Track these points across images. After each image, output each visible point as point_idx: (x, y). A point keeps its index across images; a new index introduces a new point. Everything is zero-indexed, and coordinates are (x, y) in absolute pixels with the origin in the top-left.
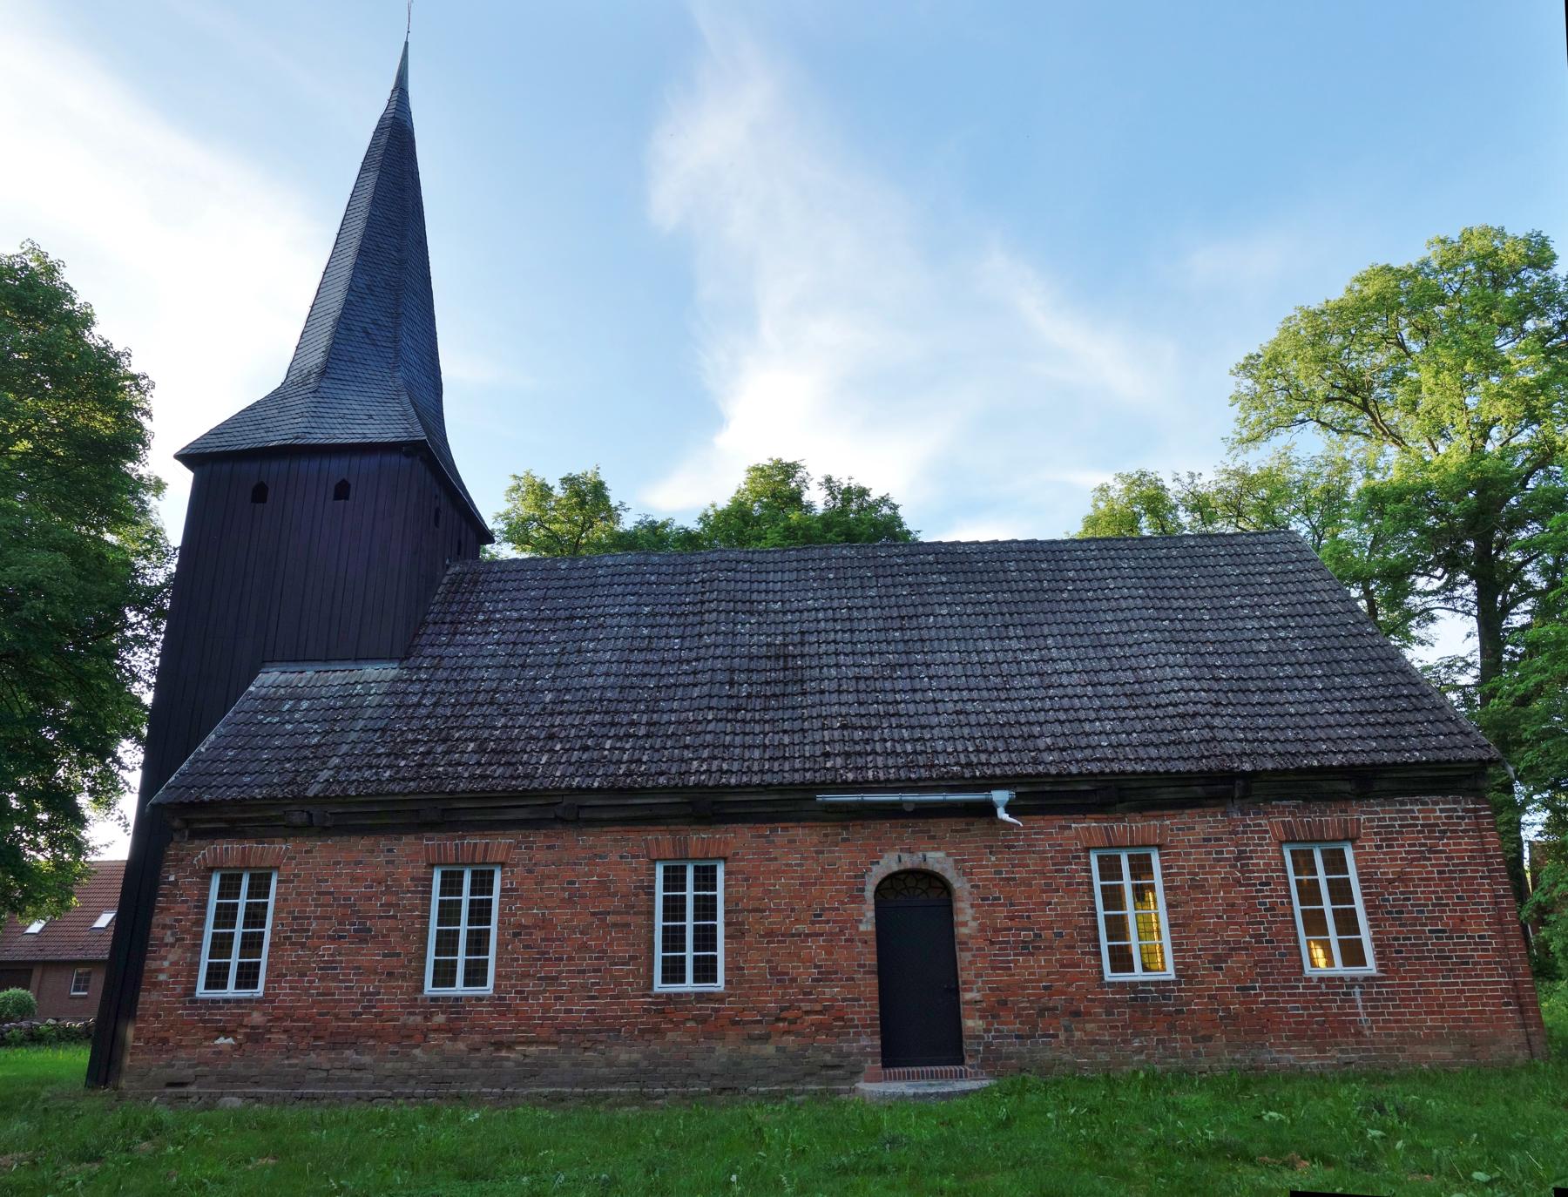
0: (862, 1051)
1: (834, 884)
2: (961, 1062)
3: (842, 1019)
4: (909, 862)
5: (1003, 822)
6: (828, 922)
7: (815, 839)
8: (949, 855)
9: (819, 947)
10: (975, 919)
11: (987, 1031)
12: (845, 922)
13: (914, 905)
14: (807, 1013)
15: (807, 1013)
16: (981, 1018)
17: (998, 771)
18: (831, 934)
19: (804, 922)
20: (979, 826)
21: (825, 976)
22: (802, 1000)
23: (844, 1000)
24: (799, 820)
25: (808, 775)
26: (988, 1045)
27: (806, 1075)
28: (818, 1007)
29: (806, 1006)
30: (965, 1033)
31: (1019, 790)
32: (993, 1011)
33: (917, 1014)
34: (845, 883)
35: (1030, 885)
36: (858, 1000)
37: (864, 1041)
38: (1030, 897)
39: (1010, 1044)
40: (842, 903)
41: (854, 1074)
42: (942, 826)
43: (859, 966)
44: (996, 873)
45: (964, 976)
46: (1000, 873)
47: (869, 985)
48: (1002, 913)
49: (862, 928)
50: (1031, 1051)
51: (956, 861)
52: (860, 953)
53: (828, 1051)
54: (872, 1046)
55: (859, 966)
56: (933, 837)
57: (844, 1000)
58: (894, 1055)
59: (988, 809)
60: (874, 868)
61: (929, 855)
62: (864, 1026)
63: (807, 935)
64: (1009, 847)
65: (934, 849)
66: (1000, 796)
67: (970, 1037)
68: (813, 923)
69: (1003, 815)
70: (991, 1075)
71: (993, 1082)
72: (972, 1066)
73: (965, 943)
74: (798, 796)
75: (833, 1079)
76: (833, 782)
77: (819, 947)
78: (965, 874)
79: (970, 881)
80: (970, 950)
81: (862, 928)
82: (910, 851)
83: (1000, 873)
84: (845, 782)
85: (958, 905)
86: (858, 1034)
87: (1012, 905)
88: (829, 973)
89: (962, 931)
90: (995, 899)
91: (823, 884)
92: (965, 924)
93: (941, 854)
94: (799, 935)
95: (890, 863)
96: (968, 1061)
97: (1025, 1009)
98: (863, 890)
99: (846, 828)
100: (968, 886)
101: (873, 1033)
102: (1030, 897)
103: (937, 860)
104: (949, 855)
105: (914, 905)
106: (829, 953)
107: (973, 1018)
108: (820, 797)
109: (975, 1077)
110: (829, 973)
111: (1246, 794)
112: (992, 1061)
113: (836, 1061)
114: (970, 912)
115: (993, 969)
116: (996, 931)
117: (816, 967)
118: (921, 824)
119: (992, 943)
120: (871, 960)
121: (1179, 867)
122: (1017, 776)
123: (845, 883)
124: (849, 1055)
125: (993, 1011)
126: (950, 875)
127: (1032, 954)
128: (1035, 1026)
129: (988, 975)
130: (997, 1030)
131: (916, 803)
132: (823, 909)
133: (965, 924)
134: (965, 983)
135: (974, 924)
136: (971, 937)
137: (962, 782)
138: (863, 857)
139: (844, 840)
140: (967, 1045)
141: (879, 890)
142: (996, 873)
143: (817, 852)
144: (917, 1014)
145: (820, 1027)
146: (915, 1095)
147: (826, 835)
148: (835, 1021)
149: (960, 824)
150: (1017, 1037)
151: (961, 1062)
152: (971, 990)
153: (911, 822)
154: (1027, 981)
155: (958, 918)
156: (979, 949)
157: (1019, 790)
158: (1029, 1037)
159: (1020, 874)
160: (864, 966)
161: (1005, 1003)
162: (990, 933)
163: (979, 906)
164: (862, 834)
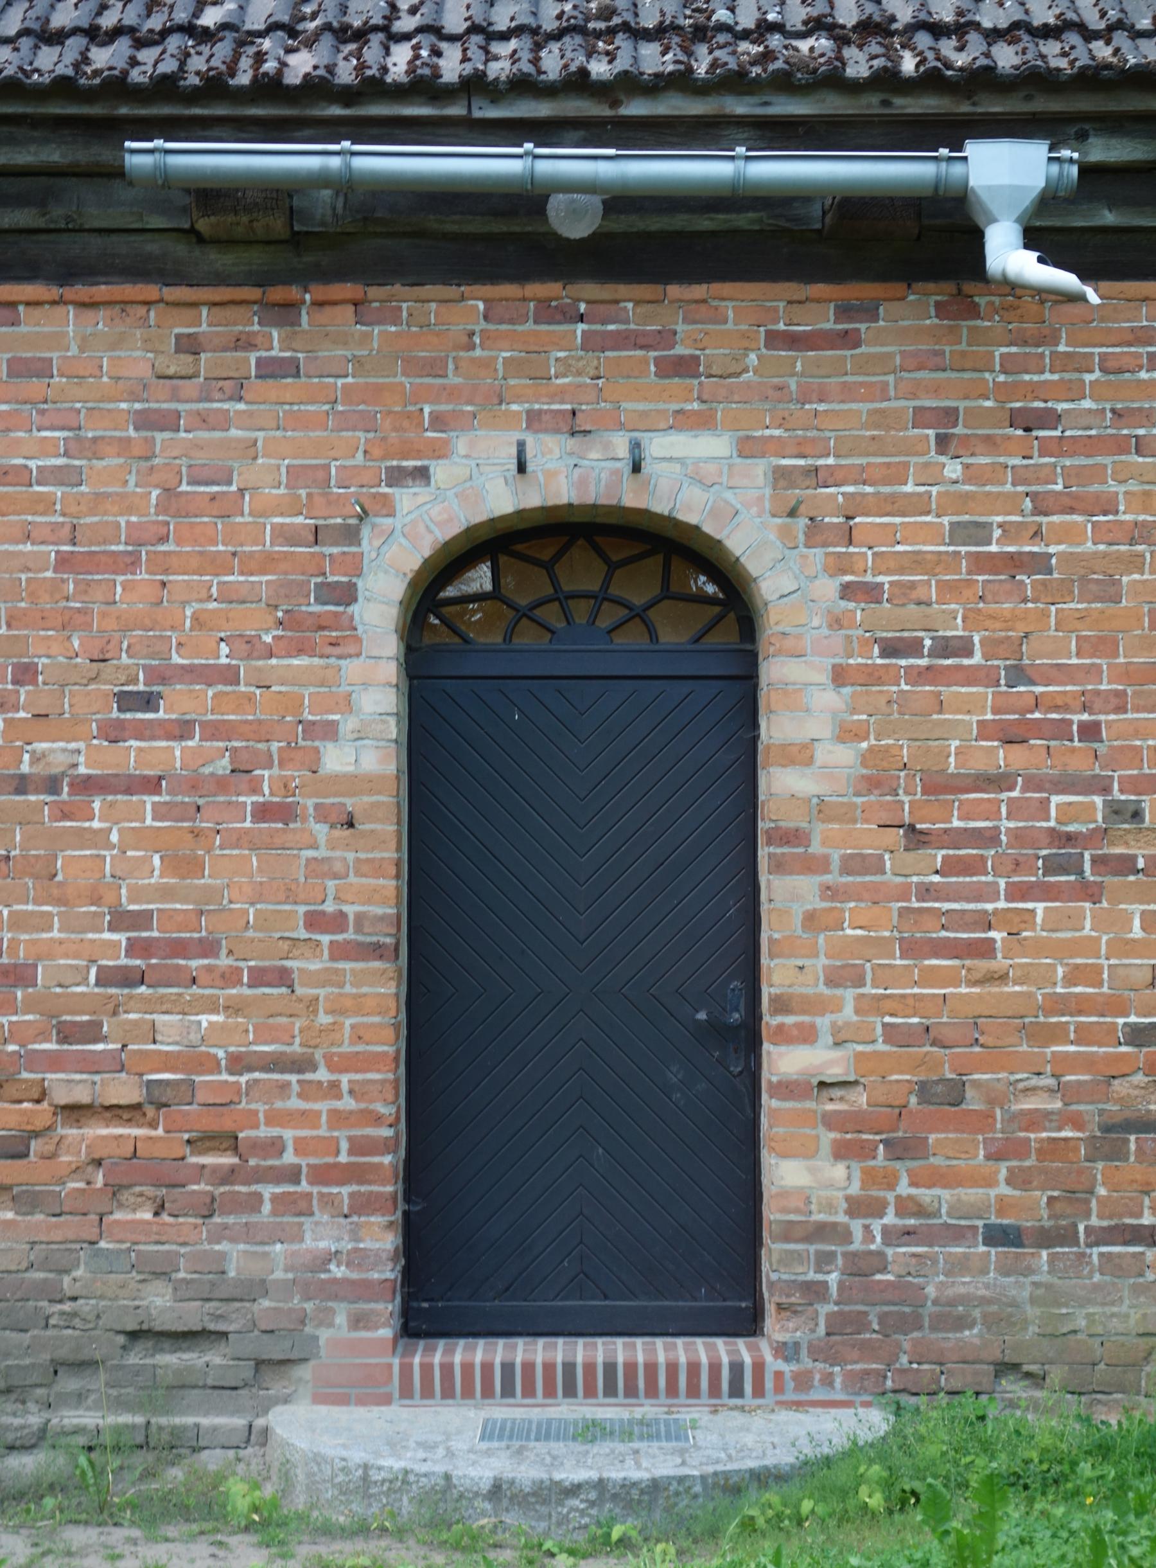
0: (312, 1279)
1: (218, 564)
2: (749, 1323)
3: (231, 1143)
4: (570, 475)
5: (1012, 287)
6: (181, 730)
7: (138, 361)
8: (748, 448)
9: (140, 837)
10: (847, 734)
11: (859, 1207)
12: (260, 731)
13: (579, 683)
14: (75, 1112)
15: (75, 1112)
16: (841, 1152)
17: (1006, 57)
18: (194, 784)
19: (71, 729)
20: (904, 321)
21: (157, 960)
22: (55, 1062)
23: (238, 1063)
24: (68, 272)
25: (101, 57)
26: (861, 1267)
27: (56, 1368)
28: (123, 1090)
29: (71, 1087)
30: (771, 1213)
31: (1105, 150)
32: (885, 1136)
33: (566, 1124)
34: (267, 562)
35: (1110, 592)
36: (302, 1065)
37: (321, 1236)
38: (1105, 646)
39: (960, 1266)
40: (251, 647)
41: (269, 1368)
42: (729, 320)
43: (315, 921)
44: (960, 533)
45: (778, 975)
46: (978, 532)
47: (360, 1009)
48: (972, 707)
49: (336, 759)
50: (1048, 1296)
51: (781, 476)
52: (319, 869)
53: (161, 1272)
54: (357, 1258)
55: (315, 921)
56: (685, 367)
57: (238, 1063)
58: (457, 1276)
59: (934, 243)
60: (406, 498)
61: (658, 446)
62: (321, 1175)
63: (88, 786)
64: (1028, 422)
65: (684, 422)
66: (1006, 172)
67: (788, 1233)
68: (114, 733)
69: (1008, 255)
70: (868, 1387)
71: (873, 1422)
72: (785, 1351)
73: (795, 837)
74: (53, 155)
75: (181, 1386)
76: (215, 86)
77: (140, 837)
78: (815, 533)
79: (840, 565)
80: (815, 865)
81: (336, 759)
82: (573, 426)
83: (978, 532)
84: (270, 87)
85: (776, 671)
86: (297, 1206)
87: (1018, 675)
88: (180, 948)
89: (782, 786)
90: (945, 648)
91: (162, 564)
92: (800, 755)
93: (712, 446)
94: (52, 785)
95: (479, 480)
96: (771, 1322)
97: (1034, 1120)
98: (347, 595)
99: (286, 313)
100: (828, 587)
101: (362, 1205)
102: (1105, 646)
103: (694, 470)
104: (748, 448)
105: (579, 683)
106: (183, 865)
107: (807, 1152)
108: (142, 155)
109: (800, 1395)
110: (180, 948)
111: (293, 1063)
112: (875, 1332)
113: (193, 1316)
114: (829, 700)
115: (911, 949)
116: (939, 786)
117: (121, 920)
118: (632, 306)
119: (916, 838)
120: (369, 885)
121: (1063, 363)
122: (1091, 78)
123: (267, 562)
124: (254, 1289)
125: (885, 1136)
126: (751, 536)
127: (1091, 893)
128: (1078, 1196)
129: (884, 975)
130: (905, 1207)
131: (620, 201)
132: (160, 676)
133: (800, 755)
134: (782, 1005)
135: (843, 757)
136: (822, 809)
137: (832, 104)
138: (350, 455)
139: (271, 370)
140: (778, 1263)
141: (430, 598)
142: (960, 533)
143: (147, 421)
144: (566, 1124)
145: (124, 1175)
146: (497, 1491)
147: (190, 346)
148: (200, 1149)
149: (815, 308)
150: (998, 1236)
151: (749, 1323)
152: (807, 1036)
153: (586, 293)
154: (1059, 1004)
155: (776, 728)
156: (854, 864)
157: (1105, 150)
158: (1046, 1238)
159: (1073, 540)
160: (338, 922)
161: (955, 1094)
162: (917, 808)
163: (872, 677)
164: (353, 341)
